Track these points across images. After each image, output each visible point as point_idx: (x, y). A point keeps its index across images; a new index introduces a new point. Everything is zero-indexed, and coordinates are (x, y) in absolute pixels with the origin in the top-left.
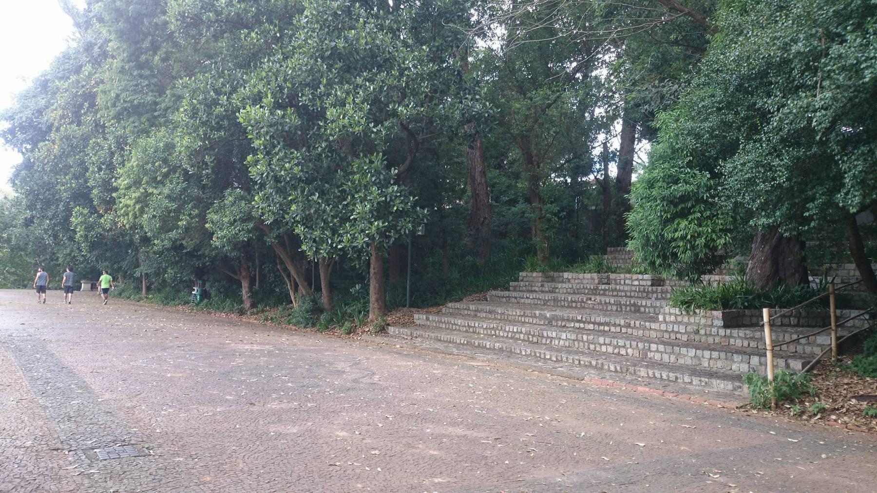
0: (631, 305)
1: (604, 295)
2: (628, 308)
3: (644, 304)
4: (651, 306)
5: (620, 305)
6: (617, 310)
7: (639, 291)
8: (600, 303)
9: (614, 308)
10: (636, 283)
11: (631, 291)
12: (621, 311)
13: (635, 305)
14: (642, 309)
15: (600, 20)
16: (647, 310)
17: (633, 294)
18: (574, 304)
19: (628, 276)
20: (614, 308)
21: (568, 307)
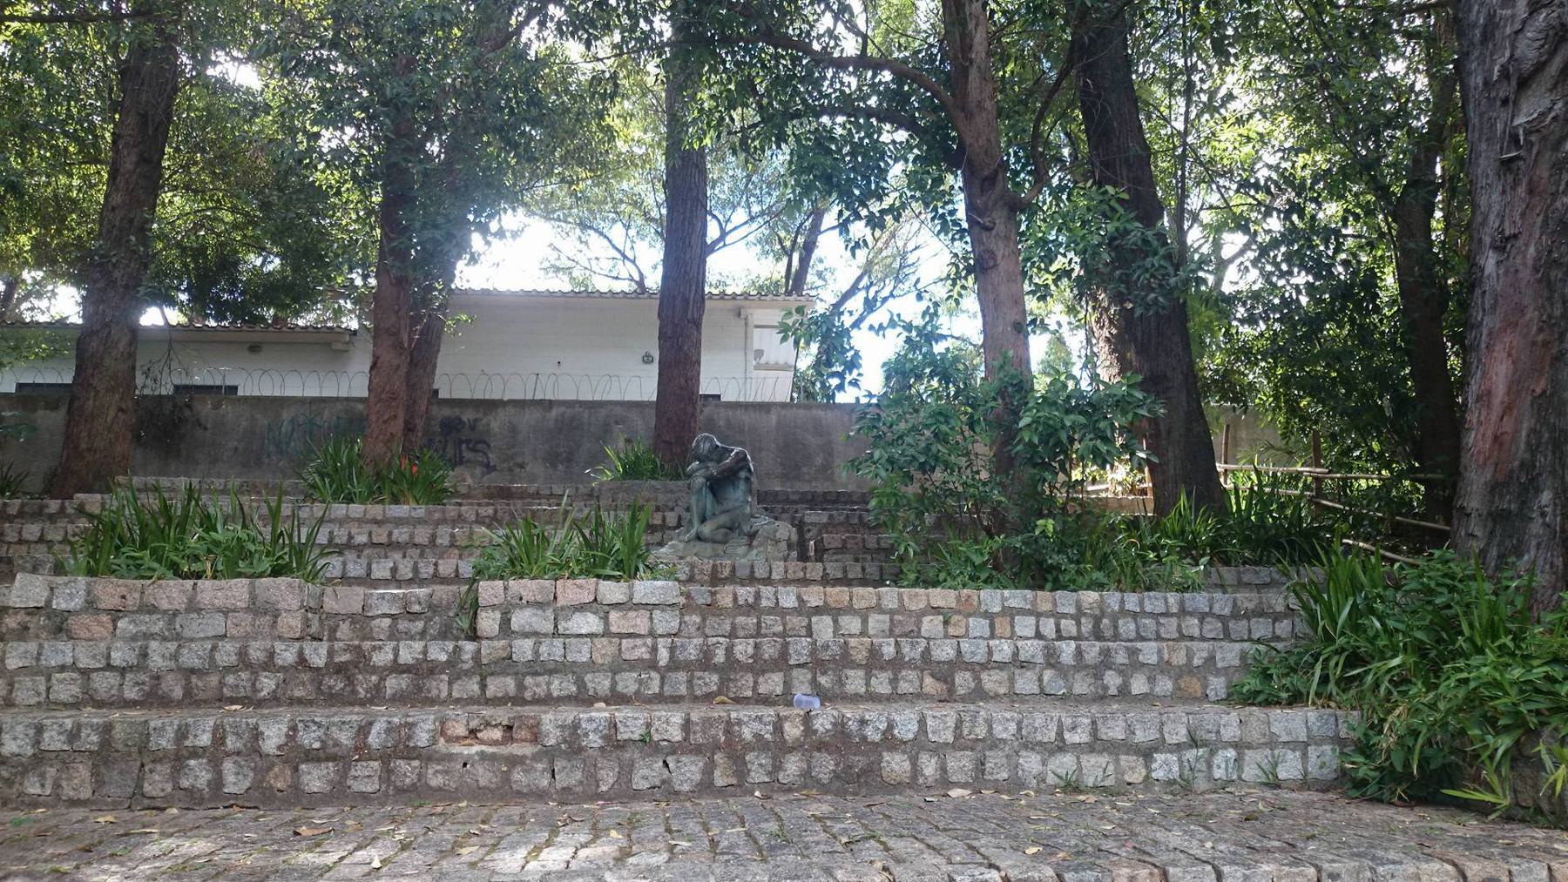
0: (813, 744)
1: (416, 697)
2: (793, 766)
3: (906, 727)
4: (960, 742)
5: (736, 751)
6: (706, 786)
7: (674, 665)
8: (573, 745)
9: (688, 771)
10: (588, 623)
11: (618, 666)
12: (741, 786)
13: (840, 742)
14: (896, 764)
15: (1166, 657)
16: (929, 767)
17: (628, 683)
18: (315, 779)
19: (527, 588)
20: (688, 771)
21: (261, 797)
